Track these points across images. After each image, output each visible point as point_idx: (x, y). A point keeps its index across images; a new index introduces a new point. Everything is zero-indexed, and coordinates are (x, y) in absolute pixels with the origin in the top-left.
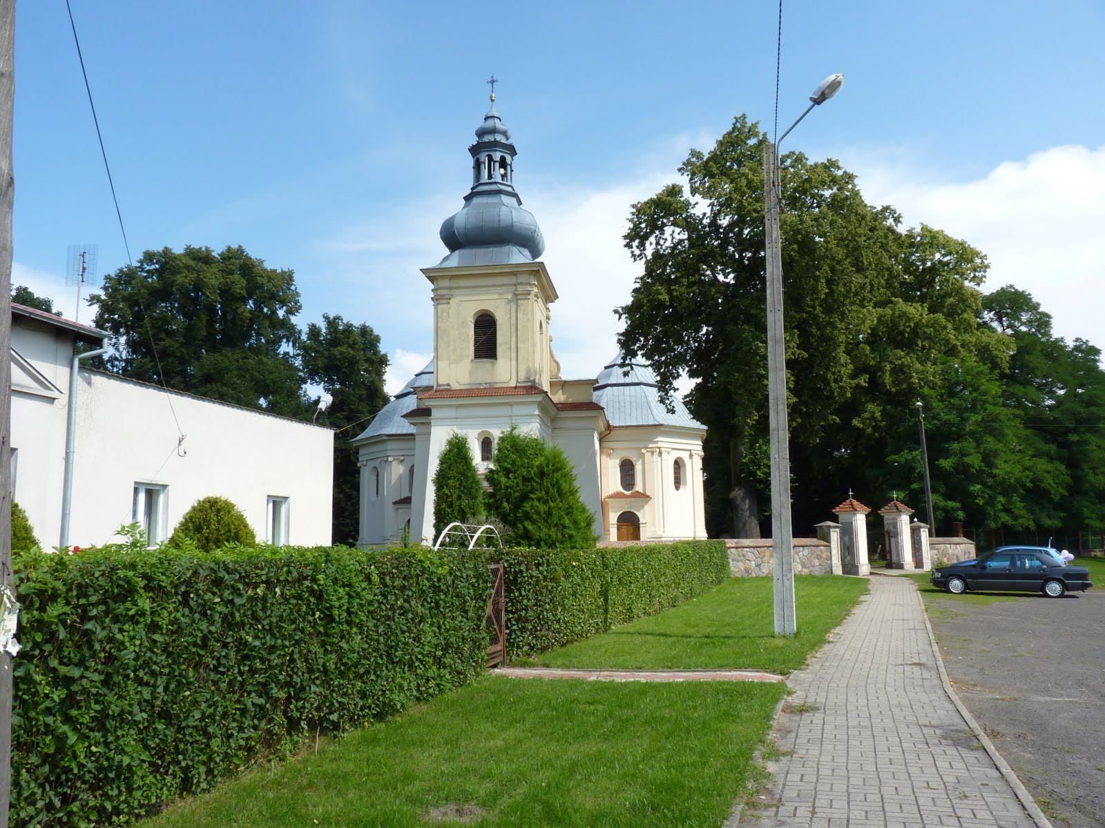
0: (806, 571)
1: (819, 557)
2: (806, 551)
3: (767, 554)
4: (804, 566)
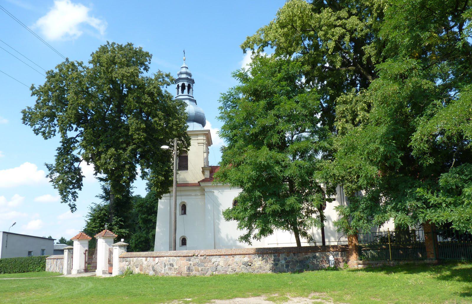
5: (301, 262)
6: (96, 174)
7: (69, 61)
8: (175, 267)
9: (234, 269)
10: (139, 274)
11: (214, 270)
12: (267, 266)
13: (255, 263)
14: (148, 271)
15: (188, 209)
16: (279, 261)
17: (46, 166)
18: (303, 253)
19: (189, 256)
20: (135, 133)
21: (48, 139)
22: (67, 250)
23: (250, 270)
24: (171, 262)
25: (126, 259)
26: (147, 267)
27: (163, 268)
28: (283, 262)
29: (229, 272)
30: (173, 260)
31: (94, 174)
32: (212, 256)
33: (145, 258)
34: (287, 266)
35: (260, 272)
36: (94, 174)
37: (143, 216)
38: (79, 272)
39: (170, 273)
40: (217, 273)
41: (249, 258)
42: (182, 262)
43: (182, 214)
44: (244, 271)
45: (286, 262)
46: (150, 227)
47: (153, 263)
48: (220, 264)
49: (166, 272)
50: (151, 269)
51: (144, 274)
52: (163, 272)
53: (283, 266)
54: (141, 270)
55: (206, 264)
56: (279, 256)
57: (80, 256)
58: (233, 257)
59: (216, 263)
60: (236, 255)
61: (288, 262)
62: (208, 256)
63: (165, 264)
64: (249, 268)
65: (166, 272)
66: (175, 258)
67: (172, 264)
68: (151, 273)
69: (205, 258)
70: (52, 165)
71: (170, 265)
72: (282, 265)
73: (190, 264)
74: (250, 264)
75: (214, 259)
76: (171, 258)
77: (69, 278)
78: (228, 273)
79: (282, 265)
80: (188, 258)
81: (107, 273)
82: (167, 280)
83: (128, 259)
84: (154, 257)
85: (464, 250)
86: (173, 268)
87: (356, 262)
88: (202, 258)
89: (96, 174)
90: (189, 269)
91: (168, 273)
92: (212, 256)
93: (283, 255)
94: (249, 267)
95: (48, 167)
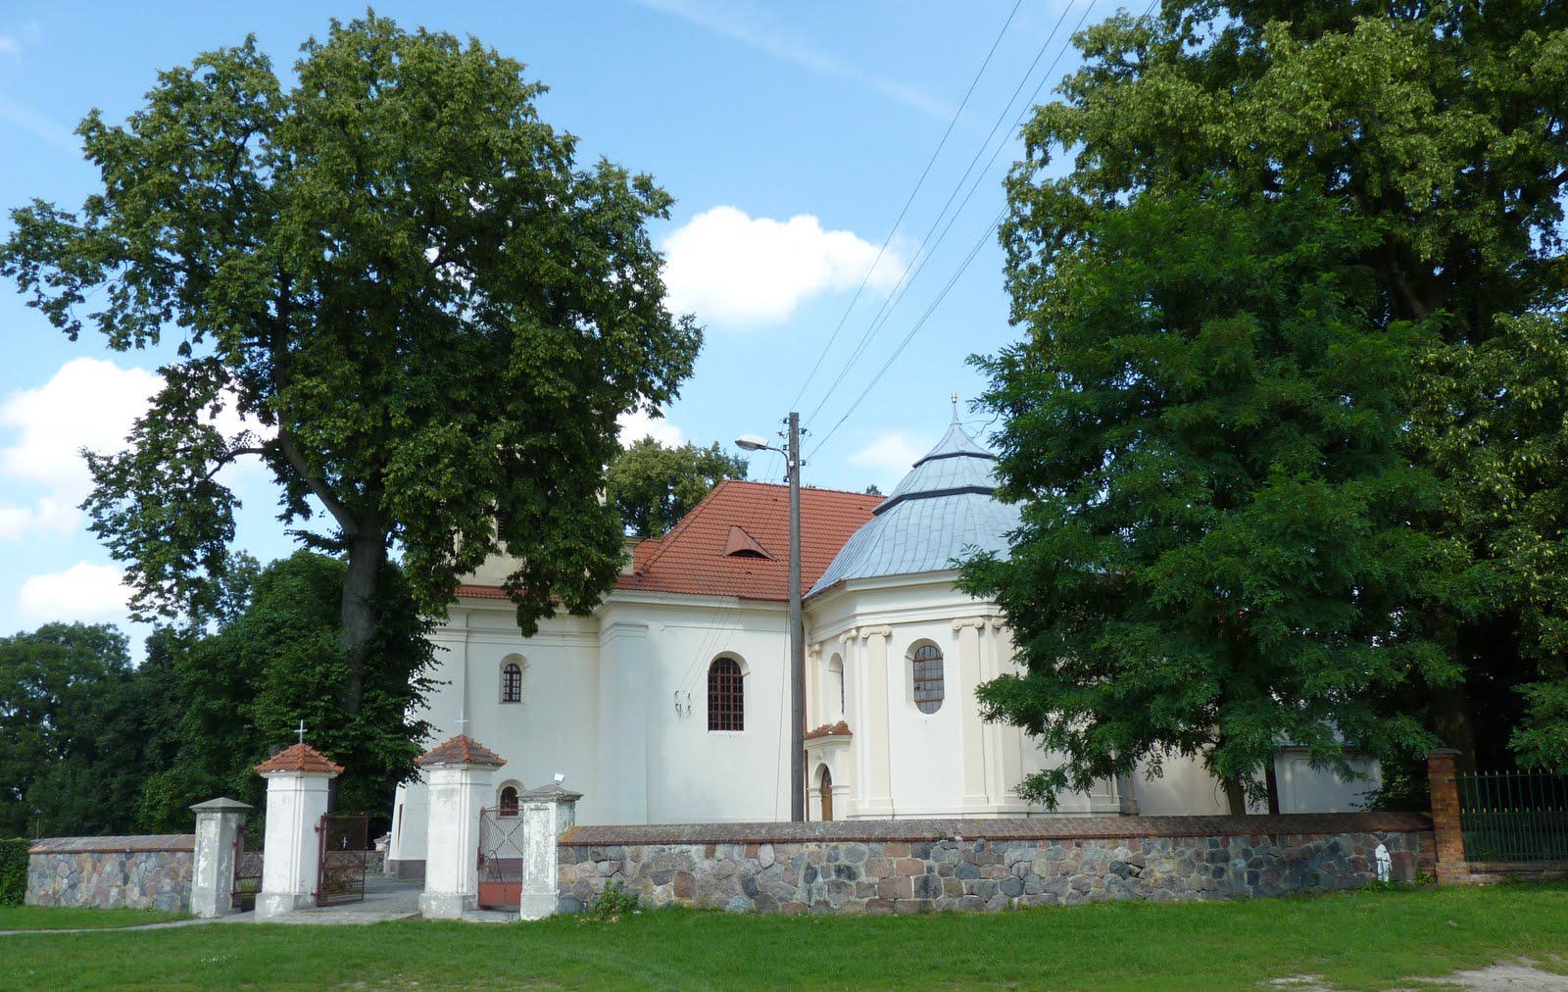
0: (145, 902)
1: (173, 874)
2: (153, 859)
3: (88, 866)
4: (143, 893)
5: (1298, 863)
6: (287, 517)
7: (253, 49)
8: (863, 878)
9: (1085, 889)
10: (671, 909)
11: (1014, 892)
12: (1193, 875)
13: (1152, 867)
14: (717, 895)
15: (529, 682)
16: (1227, 859)
17: (86, 462)
18: (1300, 837)
19: (923, 840)
20: (540, 374)
21: (132, 350)
22: (219, 815)
23: (1137, 890)
24: (844, 861)
25: (600, 849)
26: (713, 881)
27: (801, 883)
28: (1241, 863)
29: (1067, 895)
30: (850, 853)
31: (281, 518)
32: (1005, 839)
33: (702, 848)
34: (1253, 879)
35: (1171, 897)
36: (281, 518)
37: (215, 705)
38: (299, 906)
39: (836, 902)
40: (1025, 900)
41: (1132, 848)
42: (895, 860)
43: (505, 700)
44: (1117, 893)
45: (1250, 866)
46: (239, 745)
47: (749, 866)
48: (1036, 869)
49: (816, 897)
50: (738, 888)
51: (582, 909)
52: (800, 896)
53: (1242, 876)
54: (682, 892)
55: (986, 868)
56: (1227, 844)
57: (304, 841)
58: (1078, 845)
59: (1023, 865)
60: (1086, 838)
61: (1254, 865)
62: (992, 839)
63: (809, 867)
64: (1136, 883)
65: (816, 897)
66: (863, 847)
67: (848, 868)
68: (738, 903)
69: (982, 847)
70: (109, 459)
71: (839, 871)
72: (1238, 875)
73: (930, 870)
74: (1137, 870)
75: (1012, 853)
76: (842, 846)
77: (224, 924)
78: (1064, 902)
79: (1238, 875)
80: (919, 846)
81: (475, 905)
82: (818, 926)
83: (612, 851)
84: (750, 843)
85: (1534, 837)
86: (853, 883)
87: (1464, 864)
88: (972, 847)
89: (287, 517)
90: (925, 886)
91: (826, 903)
92: (1005, 839)
93: (1239, 840)
94: (1131, 879)
95: (93, 466)
